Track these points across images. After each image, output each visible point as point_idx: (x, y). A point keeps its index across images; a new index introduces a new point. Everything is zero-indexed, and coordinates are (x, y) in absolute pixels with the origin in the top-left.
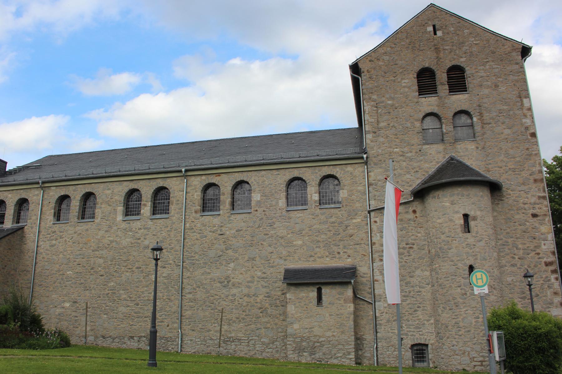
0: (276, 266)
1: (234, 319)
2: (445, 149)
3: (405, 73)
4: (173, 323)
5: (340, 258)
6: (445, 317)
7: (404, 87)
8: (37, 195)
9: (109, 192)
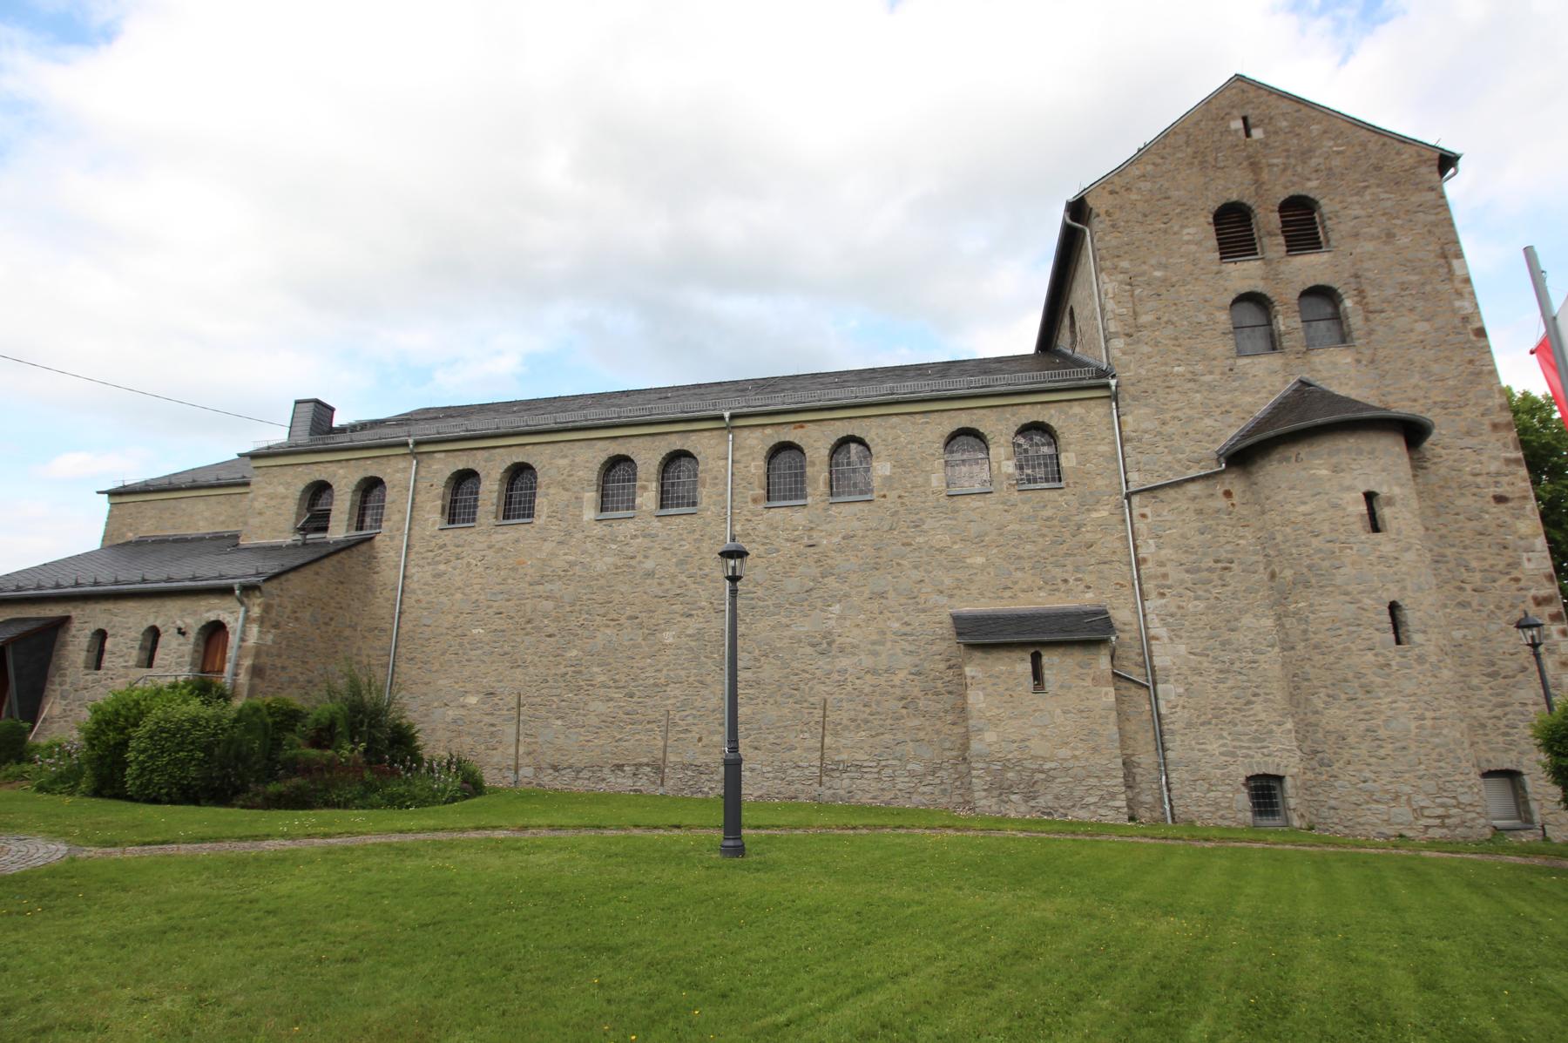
0: (930, 610)
1: (845, 722)
3: (1188, 214)
4: (711, 733)
5: (1068, 591)
6: (1335, 716)
7: (1188, 242)
9: (562, 462)
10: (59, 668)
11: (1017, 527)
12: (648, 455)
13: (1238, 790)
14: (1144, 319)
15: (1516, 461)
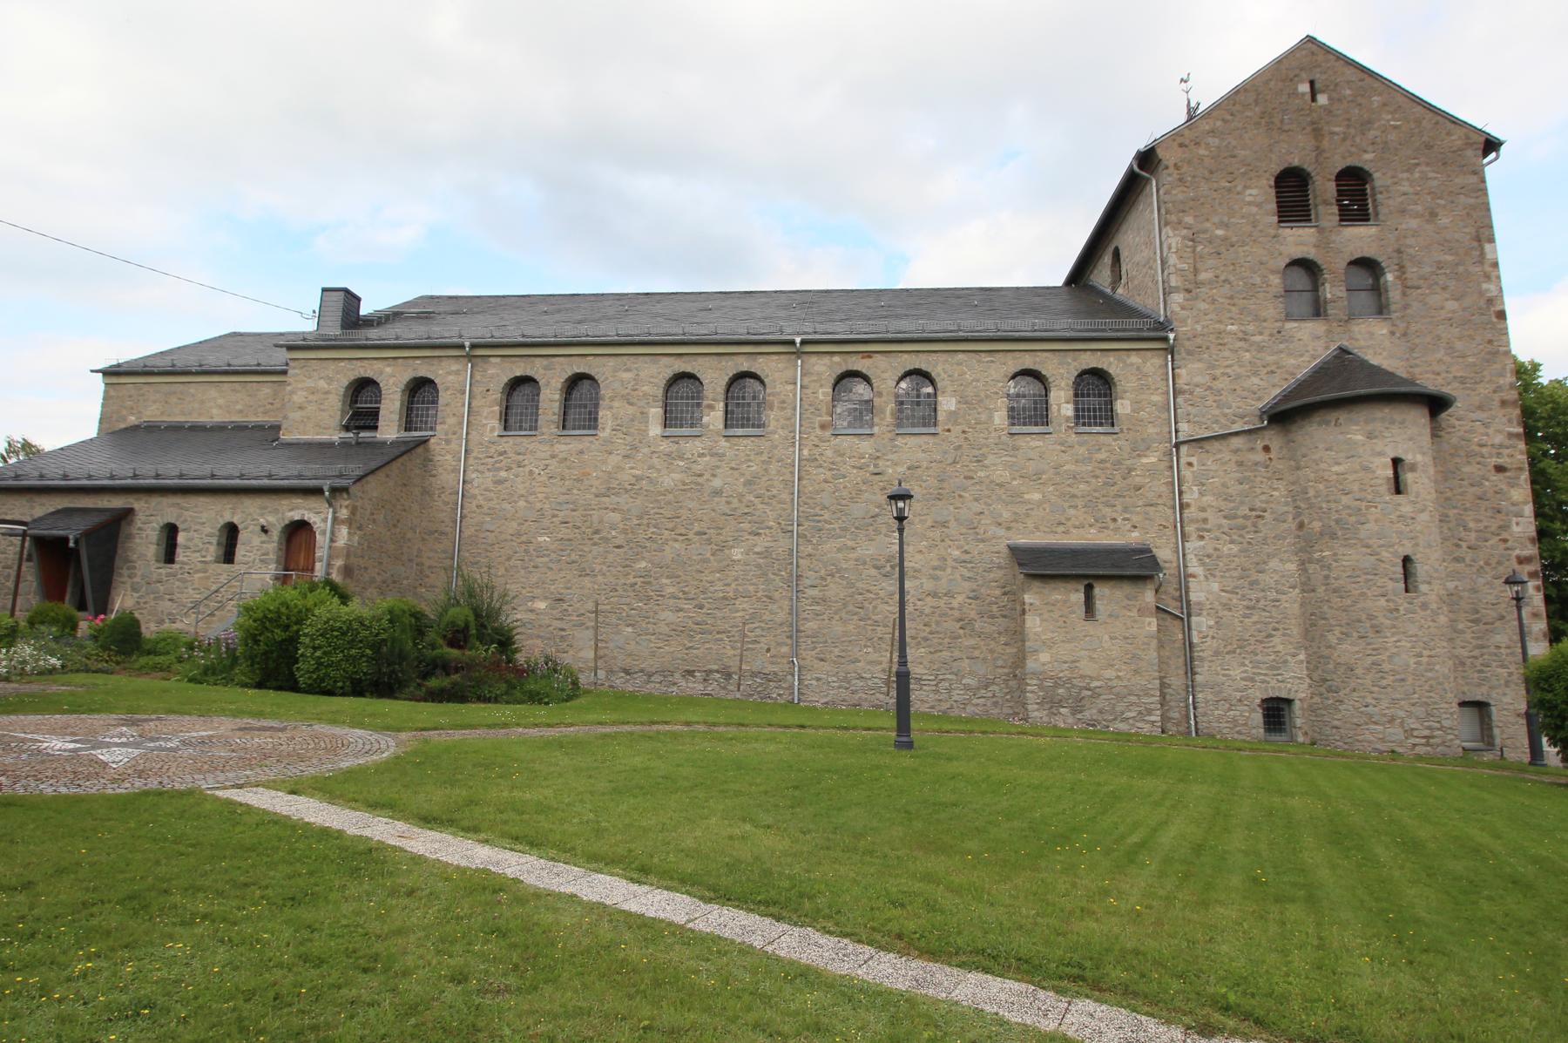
2: (1329, 332)
3: (1253, 174)
4: (779, 644)
5: (1116, 530)
6: (1347, 651)
7: (1250, 203)
8: (457, 373)
9: (626, 376)
10: (127, 560)
11: (1073, 467)
12: (714, 374)
13: (1254, 710)
14: (1203, 276)
15: (1517, 435)
